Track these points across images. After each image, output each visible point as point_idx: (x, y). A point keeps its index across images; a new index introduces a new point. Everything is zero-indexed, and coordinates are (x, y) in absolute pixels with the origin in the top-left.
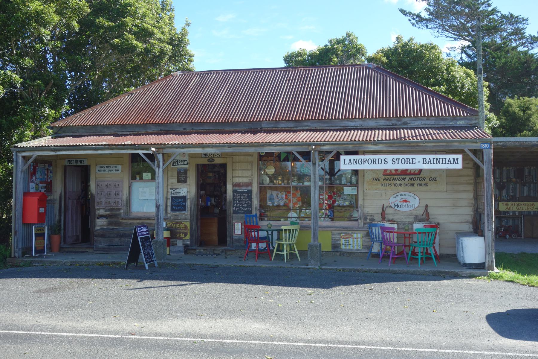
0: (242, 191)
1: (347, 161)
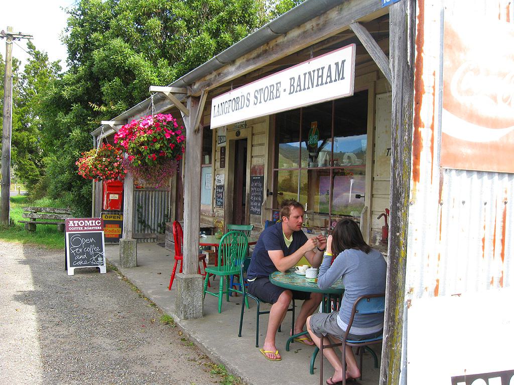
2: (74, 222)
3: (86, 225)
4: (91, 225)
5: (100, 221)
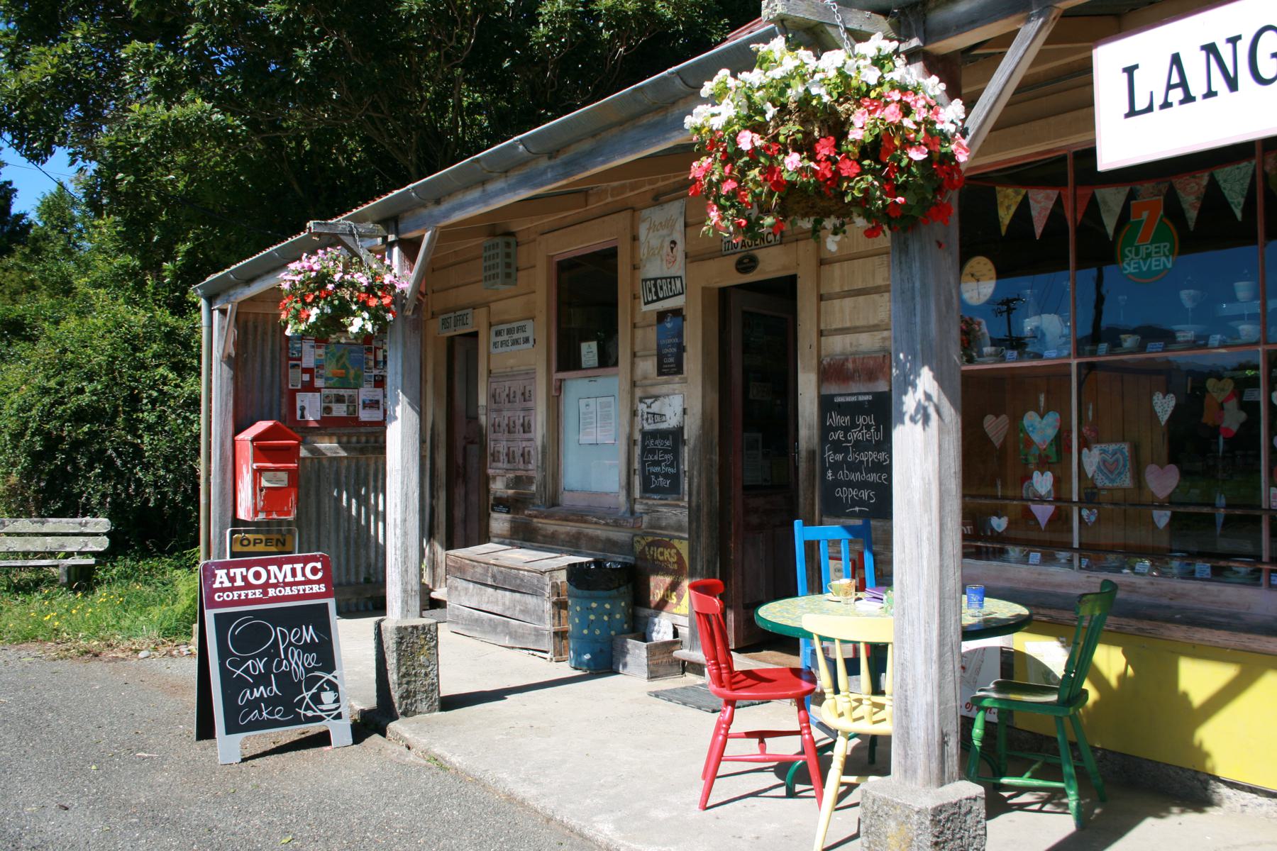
0: (853, 399)
1: (1152, 82)
2: (232, 571)
3: (273, 581)
4: (290, 579)
5: (319, 565)
